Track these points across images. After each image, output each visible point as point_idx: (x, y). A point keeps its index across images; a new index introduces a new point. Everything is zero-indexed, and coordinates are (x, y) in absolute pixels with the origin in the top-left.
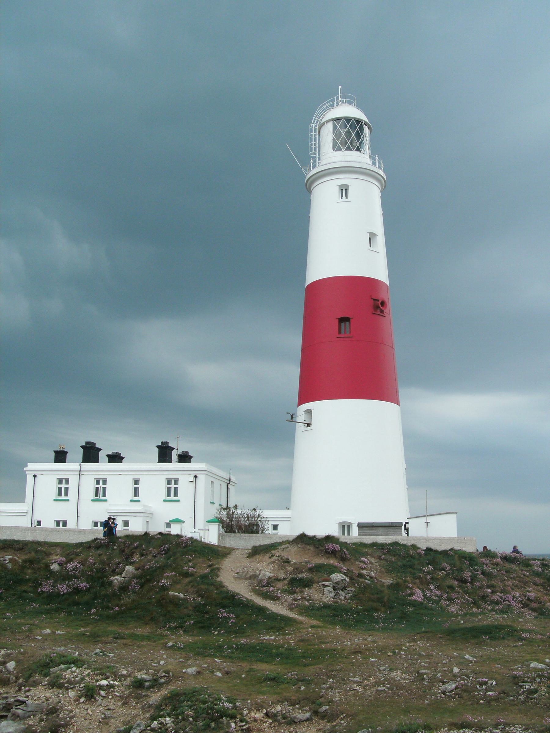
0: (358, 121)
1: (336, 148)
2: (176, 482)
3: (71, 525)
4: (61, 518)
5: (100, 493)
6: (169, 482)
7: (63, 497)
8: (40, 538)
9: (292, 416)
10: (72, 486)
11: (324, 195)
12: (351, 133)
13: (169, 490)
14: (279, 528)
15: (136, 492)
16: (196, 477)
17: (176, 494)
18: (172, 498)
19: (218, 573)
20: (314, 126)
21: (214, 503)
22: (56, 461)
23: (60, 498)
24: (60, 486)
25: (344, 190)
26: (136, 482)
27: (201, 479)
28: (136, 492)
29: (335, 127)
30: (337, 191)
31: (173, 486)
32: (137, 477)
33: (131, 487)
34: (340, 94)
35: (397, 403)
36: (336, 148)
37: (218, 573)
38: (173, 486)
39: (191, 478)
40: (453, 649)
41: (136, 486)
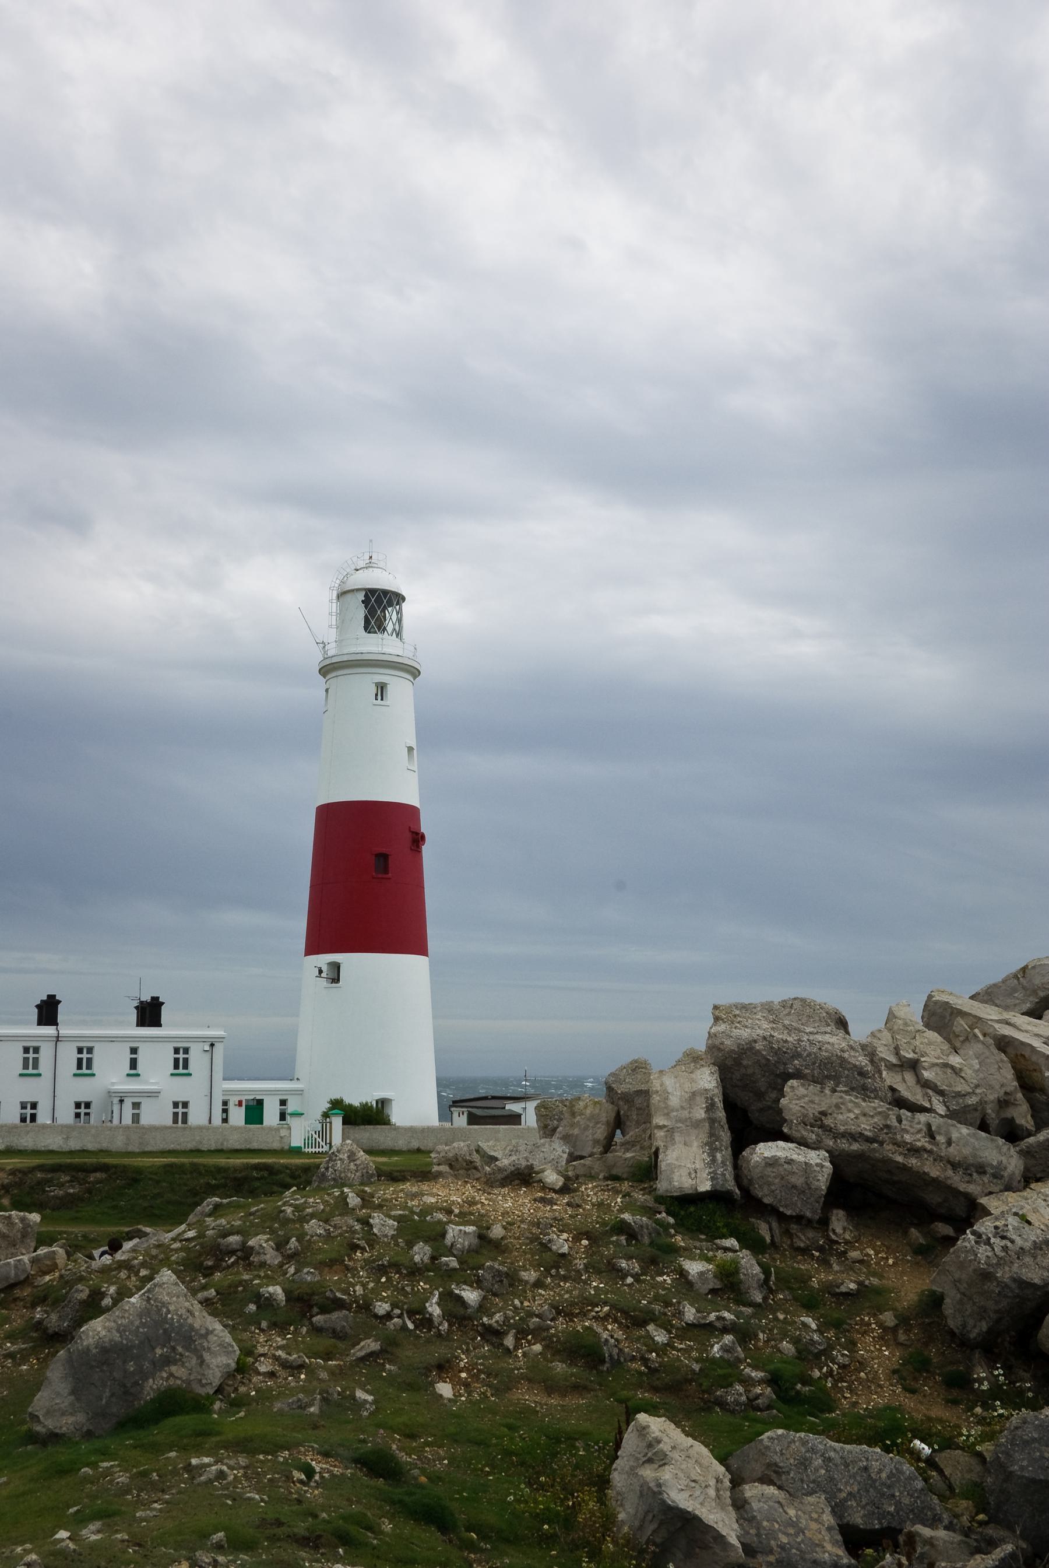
3: (43, 1117)
5: (84, 1064)
6: (177, 1051)
7: (181, 1071)
8: (187, 1143)
10: (45, 1056)
13: (176, 1061)
15: (133, 1064)
16: (212, 1045)
17: (186, 1067)
18: (84, 1071)
22: (40, 1023)
23: (80, 1072)
24: (177, 1056)
25: (381, 689)
26: (134, 1051)
27: (219, 1049)
28: (133, 1064)
30: (373, 690)
31: (85, 1056)
32: (134, 1045)
33: (128, 1056)
38: (31, 1055)
39: (207, 1048)
40: (729, 1298)
41: (134, 1056)
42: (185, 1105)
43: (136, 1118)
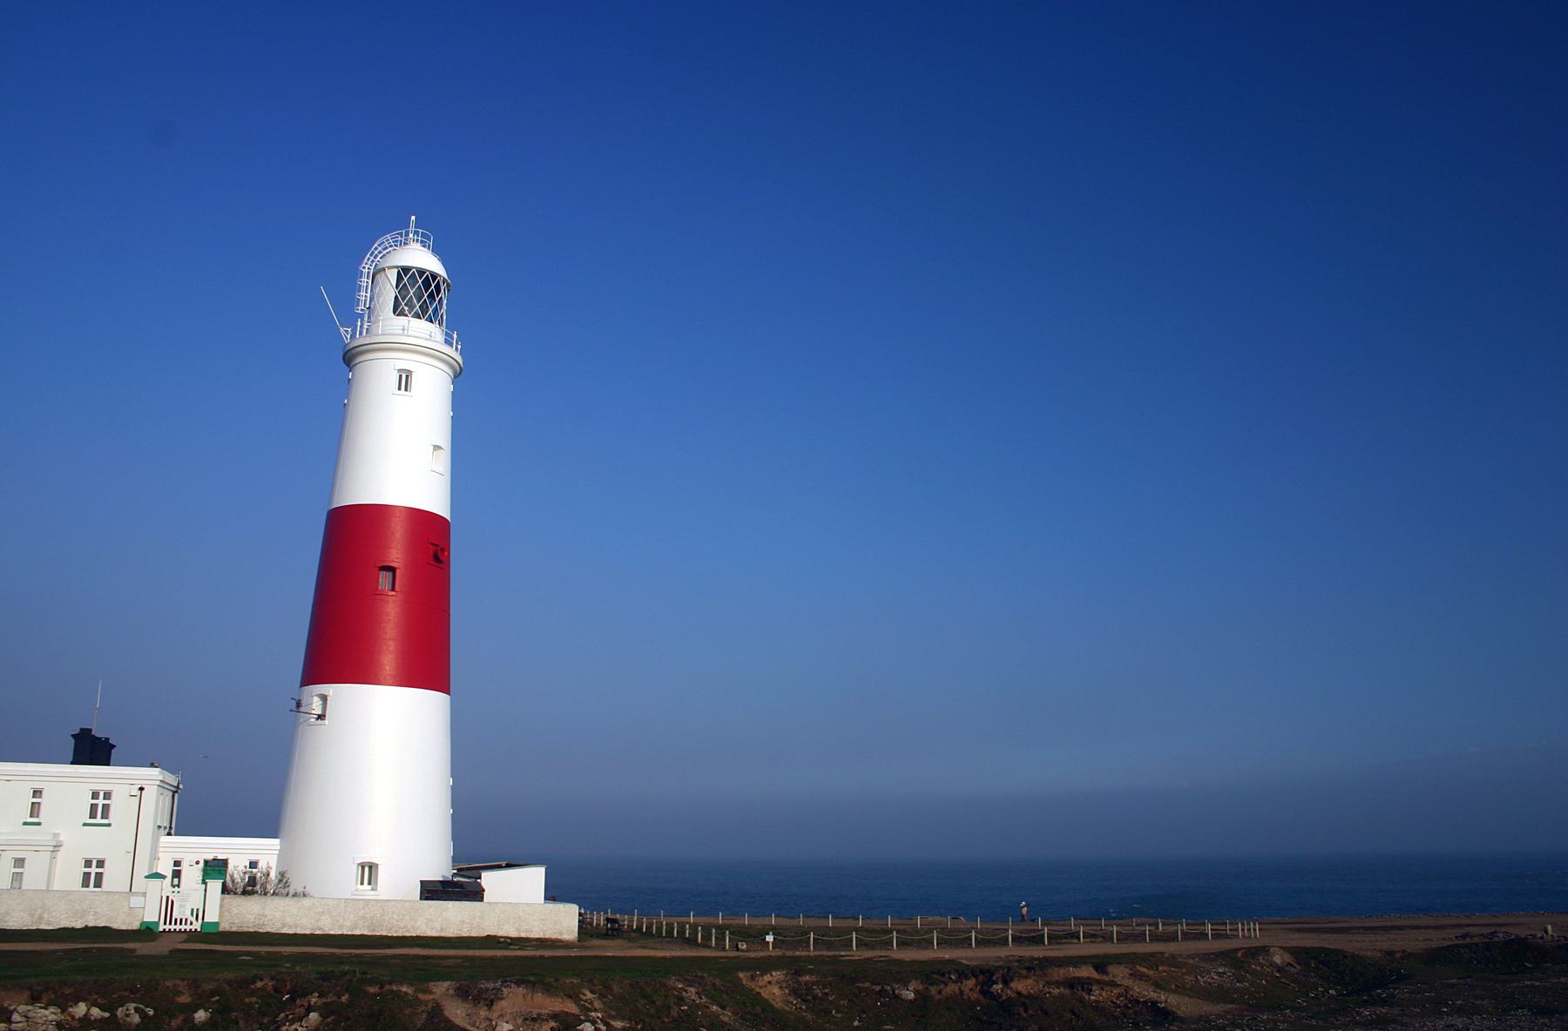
0: (434, 276)
1: (397, 310)
2: (107, 795)
4: (95, 855)
9: (299, 704)
11: (378, 373)
12: (420, 294)
14: (114, 796)
15: (35, 809)
17: (105, 815)
18: (99, 820)
19: (172, 780)
20: (367, 267)
21: (409, 374)
25: (405, 380)
26: (37, 793)
28: (35, 809)
29: (399, 278)
31: (101, 802)
32: (38, 786)
34: (412, 228)
35: (448, 692)
36: (397, 310)
37: (172, 780)
42: (101, 864)
43: (17, 877)
